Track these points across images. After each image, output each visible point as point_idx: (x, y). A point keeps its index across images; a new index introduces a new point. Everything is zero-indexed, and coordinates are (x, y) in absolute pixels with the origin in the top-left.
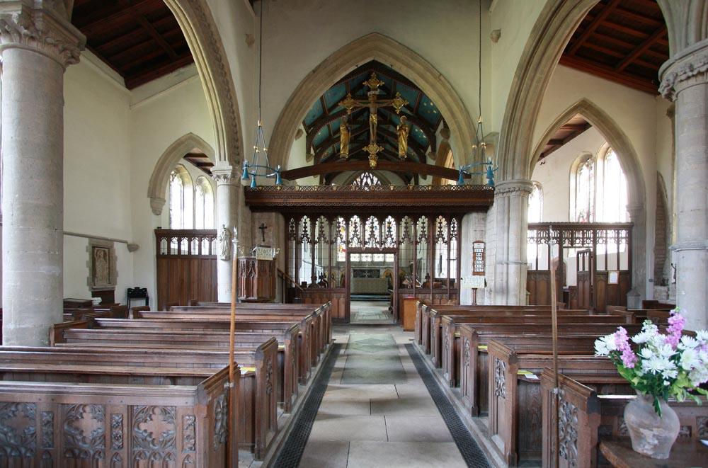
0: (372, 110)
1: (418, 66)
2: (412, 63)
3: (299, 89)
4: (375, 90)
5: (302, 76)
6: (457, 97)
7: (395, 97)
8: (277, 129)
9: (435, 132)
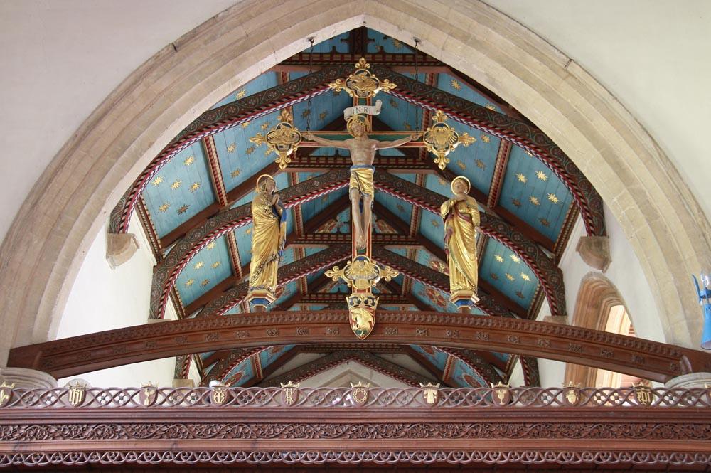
0: (358, 156)
1: (498, 39)
2: (480, 31)
3: (125, 91)
4: (370, 102)
5: (138, 56)
6: (628, 119)
7: (428, 124)
8: (35, 204)
9: (558, 259)
